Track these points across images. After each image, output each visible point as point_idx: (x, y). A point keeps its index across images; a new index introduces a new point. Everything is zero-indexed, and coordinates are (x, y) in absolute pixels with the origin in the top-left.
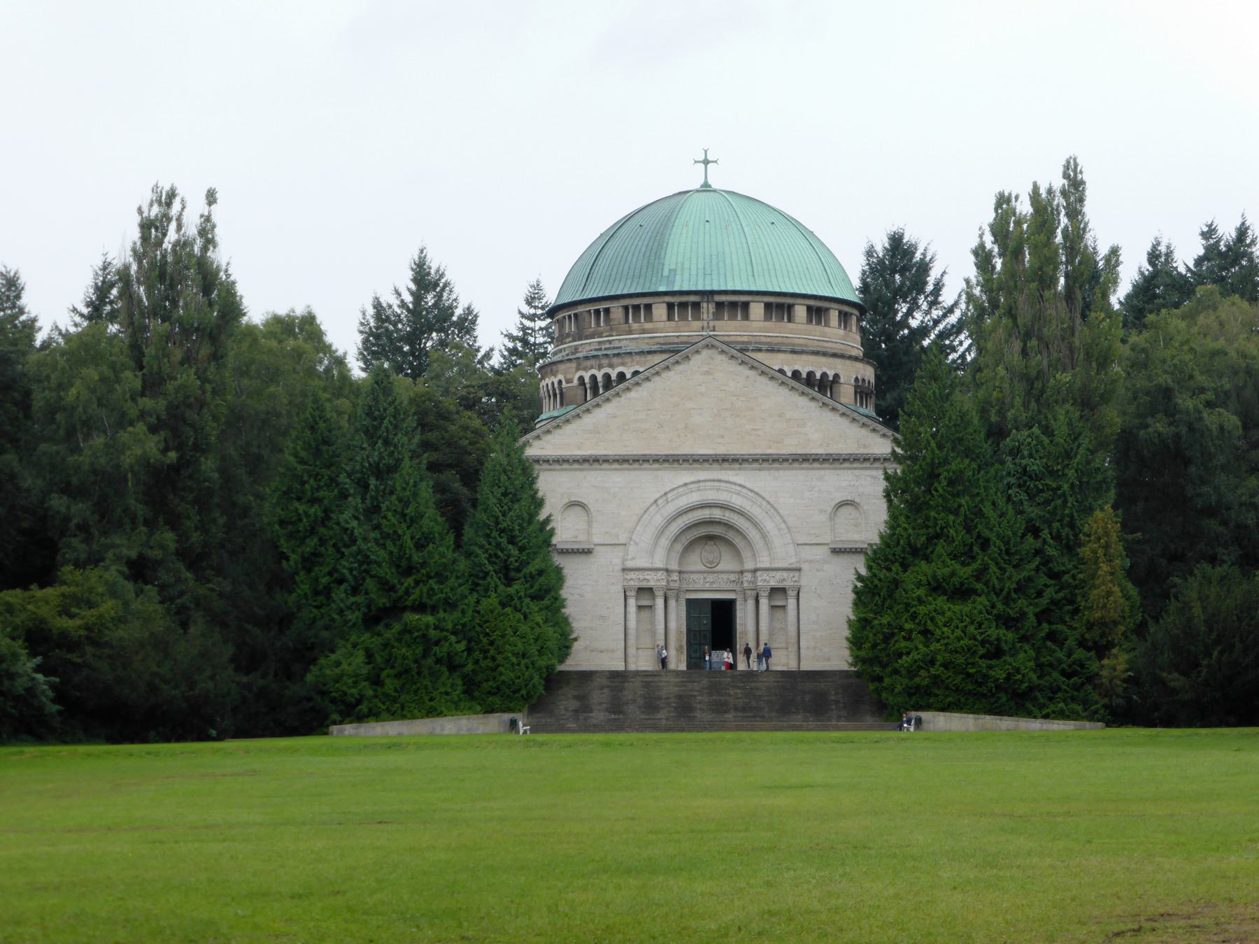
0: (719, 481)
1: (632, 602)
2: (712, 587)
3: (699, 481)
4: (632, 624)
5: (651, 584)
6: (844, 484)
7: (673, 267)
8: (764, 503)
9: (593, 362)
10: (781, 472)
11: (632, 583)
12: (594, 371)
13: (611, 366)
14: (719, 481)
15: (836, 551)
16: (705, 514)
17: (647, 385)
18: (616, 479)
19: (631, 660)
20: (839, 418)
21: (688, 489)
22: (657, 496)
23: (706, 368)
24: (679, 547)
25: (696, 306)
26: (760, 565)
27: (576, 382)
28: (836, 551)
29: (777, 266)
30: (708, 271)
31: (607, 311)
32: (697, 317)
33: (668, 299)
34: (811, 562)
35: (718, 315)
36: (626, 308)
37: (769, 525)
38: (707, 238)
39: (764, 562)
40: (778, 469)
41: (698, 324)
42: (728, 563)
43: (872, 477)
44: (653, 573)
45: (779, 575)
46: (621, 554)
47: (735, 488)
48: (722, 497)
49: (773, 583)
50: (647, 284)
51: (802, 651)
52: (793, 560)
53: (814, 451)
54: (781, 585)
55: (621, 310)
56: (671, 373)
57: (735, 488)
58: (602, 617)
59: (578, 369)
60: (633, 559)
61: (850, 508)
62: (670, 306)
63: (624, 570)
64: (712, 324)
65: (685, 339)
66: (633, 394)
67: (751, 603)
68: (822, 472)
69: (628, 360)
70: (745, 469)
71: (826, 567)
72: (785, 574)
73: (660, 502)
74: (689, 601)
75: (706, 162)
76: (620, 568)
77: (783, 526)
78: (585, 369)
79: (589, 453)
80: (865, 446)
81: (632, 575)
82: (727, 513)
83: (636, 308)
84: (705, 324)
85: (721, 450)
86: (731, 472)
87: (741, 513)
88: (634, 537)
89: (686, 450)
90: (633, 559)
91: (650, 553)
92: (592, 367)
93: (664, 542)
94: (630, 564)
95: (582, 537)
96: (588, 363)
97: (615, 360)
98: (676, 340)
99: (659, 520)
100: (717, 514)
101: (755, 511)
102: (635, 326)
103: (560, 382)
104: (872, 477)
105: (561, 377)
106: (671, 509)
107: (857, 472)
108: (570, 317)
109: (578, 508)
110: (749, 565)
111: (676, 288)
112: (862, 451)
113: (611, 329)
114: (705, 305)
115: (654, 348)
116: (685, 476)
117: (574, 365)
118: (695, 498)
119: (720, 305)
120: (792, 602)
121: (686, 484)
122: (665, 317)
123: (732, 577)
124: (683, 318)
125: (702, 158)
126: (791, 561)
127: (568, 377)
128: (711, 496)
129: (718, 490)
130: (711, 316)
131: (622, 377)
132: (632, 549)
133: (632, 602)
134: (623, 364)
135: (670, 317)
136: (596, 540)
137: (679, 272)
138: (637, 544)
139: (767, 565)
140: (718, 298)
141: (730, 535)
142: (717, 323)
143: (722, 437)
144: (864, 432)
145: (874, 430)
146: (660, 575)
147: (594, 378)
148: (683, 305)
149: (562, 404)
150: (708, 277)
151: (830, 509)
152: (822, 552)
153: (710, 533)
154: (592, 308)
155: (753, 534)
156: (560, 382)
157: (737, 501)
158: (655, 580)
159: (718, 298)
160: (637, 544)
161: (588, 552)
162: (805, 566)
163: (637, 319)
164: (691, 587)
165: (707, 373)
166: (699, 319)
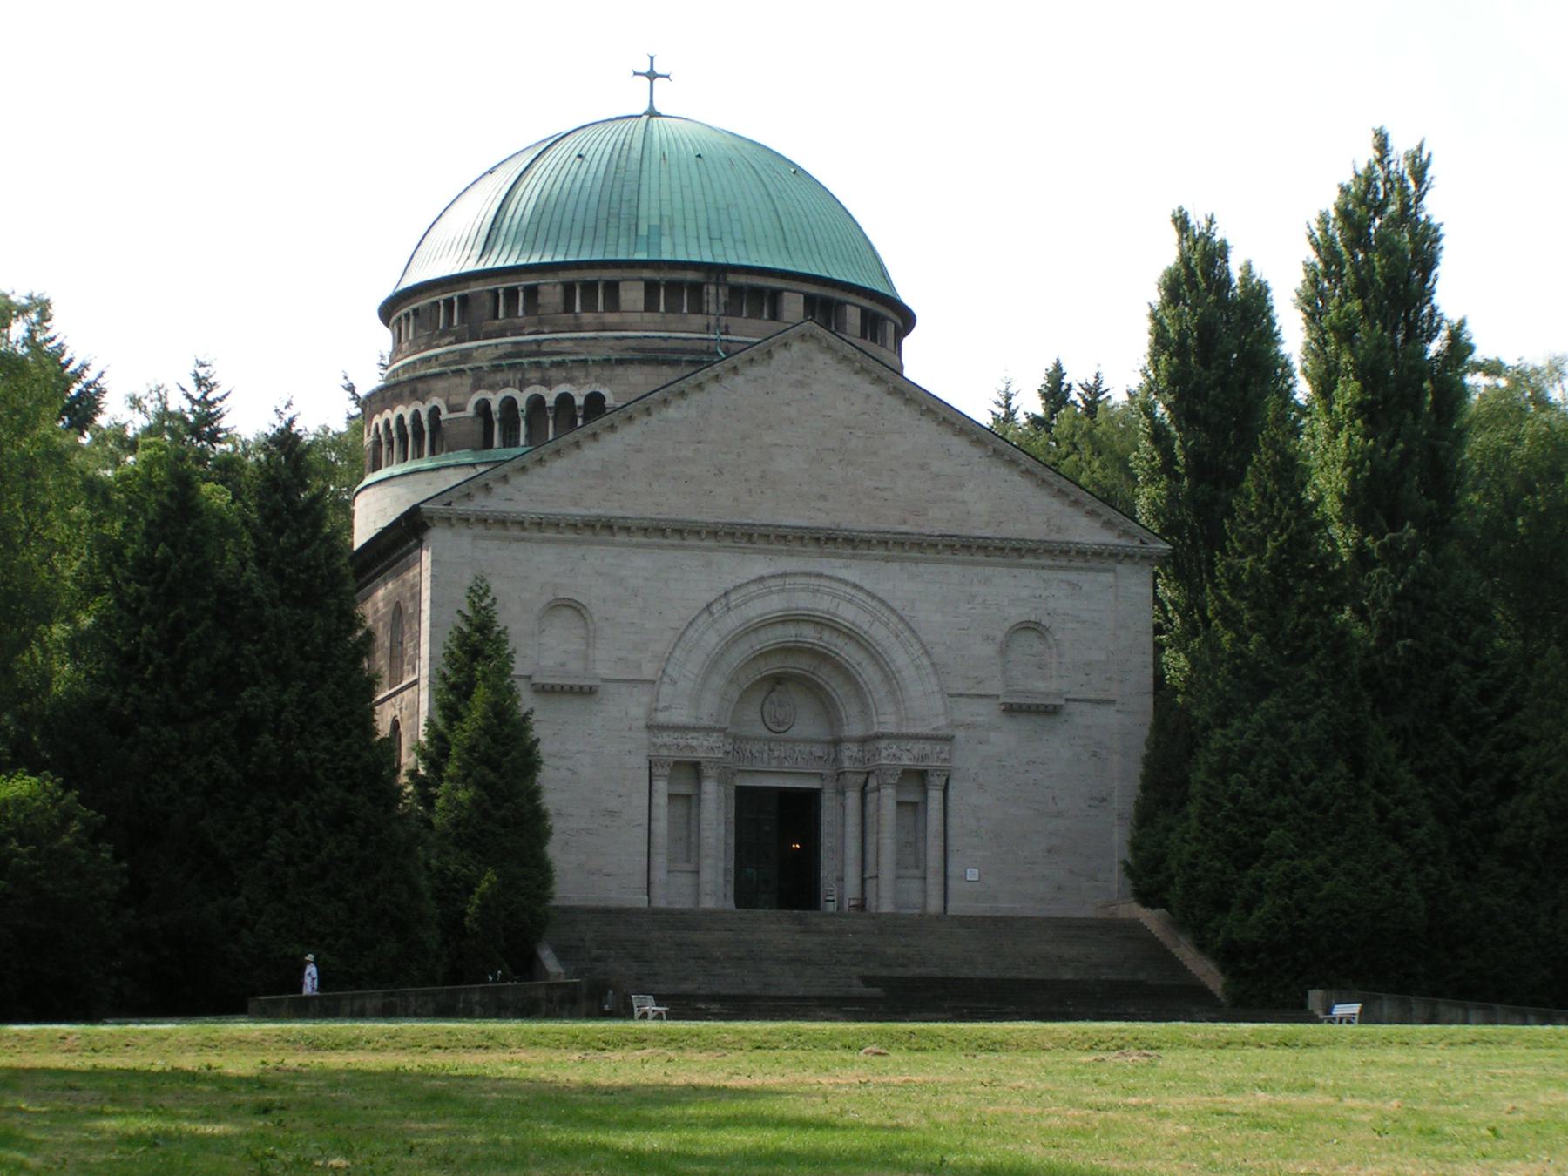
0: (820, 576)
1: (661, 786)
2: (780, 772)
3: (784, 575)
4: (661, 826)
5: (700, 755)
6: (1025, 593)
7: (655, 221)
8: (894, 619)
9: (510, 375)
10: (922, 567)
11: (665, 752)
12: (540, 390)
13: (546, 382)
14: (820, 576)
15: (1011, 710)
16: (789, 633)
17: (696, 397)
18: (639, 564)
19: (657, 891)
20: (1017, 478)
21: (762, 589)
22: (711, 597)
23: (797, 376)
24: (735, 694)
25: (696, 289)
26: (876, 729)
27: (470, 410)
28: (1011, 710)
29: (820, 241)
30: (715, 234)
31: (532, 292)
32: (697, 308)
33: (647, 274)
34: (969, 726)
35: (733, 309)
36: (569, 288)
37: (900, 659)
38: (705, 179)
39: (888, 721)
40: (916, 561)
41: (698, 320)
42: (807, 725)
43: (1069, 583)
44: (701, 736)
45: (917, 748)
46: (645, 699)
47: (846, 591)
48: (823, 605)
49: (907, 761)
50: (611, 248)
51: (951, 883)
52: (942, 722)
53: (978, 533)
54: (921, 766)
55: (559, 289)
56: (739, 379)
57: (846, 591)
58: (611, 813)
59: (476, 387)
60: (667, 708)
61: (1033, 635)
62: (651, 288)
63: (649, 727)
64: (723, 321)
65: (678, 344)
66: (671, 412)
67: (853, 798)
68: (989, 570)
69: (578, 373)
70: (862, 557)
71: (993, 736)
72: (928, 747)
73: (715, 608)
74: (742, 792)
75: (652, 76)
76: (642, 723)
77: (926, 662)
78: (493, 387)
79: (594, 512)
80: (1059, 530)
81: (666, 738)
82: (826, 635)
83: (589, 288)
84: (712, 320)
85: (822, 520)
86: (839, 562)
87: (852, 635)
88: (669, 670)
89: (764, 513)
90: (667, 708)
91: (693, 699)
92: (506, 385)
93: (717, 681)
94: (662, 717)
95: (574, 666)
96: (499, 377)
97: (553, 373)
98: (663, 345)
99: (712, 640)
100: (809, 635)
101: (879, 633)
102: (588, 317)
103: (435, 412)
104: (1069, 583)
105: (436, 401)
106: (732, 622)
107: (1045, 574)
108: (407, 315)
109: (568, 612)
110: (854, 729)
111: (666, 256)
112: (1054, 537)
113: (541, 322)
114: (712, 289)
115: (627, 355)
116: (759, 565)
117: (467, 381)
118: (775, 604)
119: (736, 291)
120: (935, 796)
121: (762, 579)
122: (641, 305)
123: (818, 751)
124: (673, 308)
125: (646, 69)
126: (939, 723)
127: (454, 400)
128: (804, 602)
129: (815, 591)
130: (722, 310)
131: (595, 401)
132: (666, 689)
133: (661, 786)
134: (570, 380)
135: (651, 306)
136: (603, 671)
137: (666, 230)
138: (673, 682)
139: (890, 728)
140: (732, 279)
141: (825, 676)
142: (733, 322)
143: (824, 497)
144: (1056, 505)
145: (1076, 503)
146: (714, 739)
147: (509, 404)
148: (674, 288)
149: (433, 452)
150: (717, 244)
151: (1000, 636)
152: (984, 712)
153: (795, 671)
154: (501, 285)
155: (869, 674)
156: (435, 412)
157: (847, 614)
158: (704, 747)
159: (732, 279)
160: (673, 682)
161: (587, 692)
162: (960, 734)
163: (589, 306)
164: (746, 766)
165: (801, 384)
166: (700, 311)
